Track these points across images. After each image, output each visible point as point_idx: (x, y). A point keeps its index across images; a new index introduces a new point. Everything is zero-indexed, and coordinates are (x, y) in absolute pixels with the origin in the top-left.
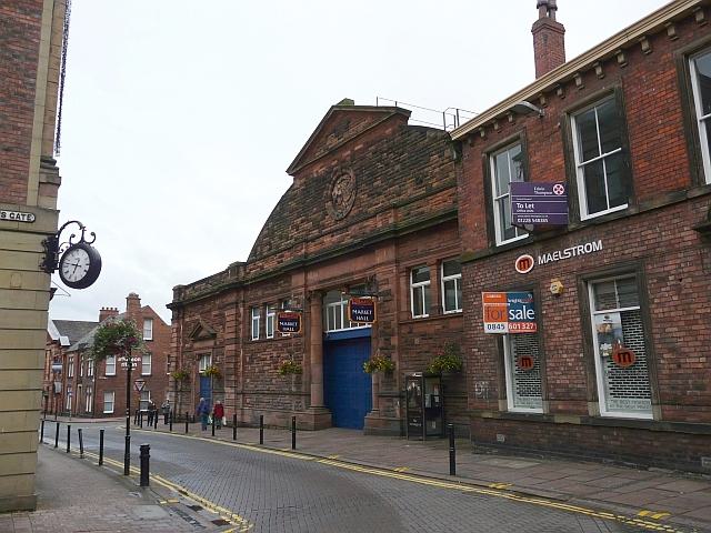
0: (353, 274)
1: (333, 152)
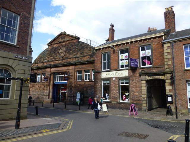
1: (60, 43)
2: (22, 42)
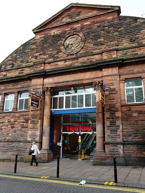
0: (83, 80)
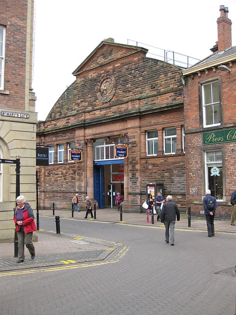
0: (113, 131)
1: (102, 66)
2: (13, 82)
